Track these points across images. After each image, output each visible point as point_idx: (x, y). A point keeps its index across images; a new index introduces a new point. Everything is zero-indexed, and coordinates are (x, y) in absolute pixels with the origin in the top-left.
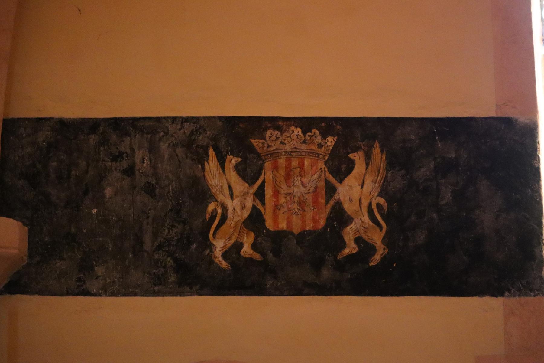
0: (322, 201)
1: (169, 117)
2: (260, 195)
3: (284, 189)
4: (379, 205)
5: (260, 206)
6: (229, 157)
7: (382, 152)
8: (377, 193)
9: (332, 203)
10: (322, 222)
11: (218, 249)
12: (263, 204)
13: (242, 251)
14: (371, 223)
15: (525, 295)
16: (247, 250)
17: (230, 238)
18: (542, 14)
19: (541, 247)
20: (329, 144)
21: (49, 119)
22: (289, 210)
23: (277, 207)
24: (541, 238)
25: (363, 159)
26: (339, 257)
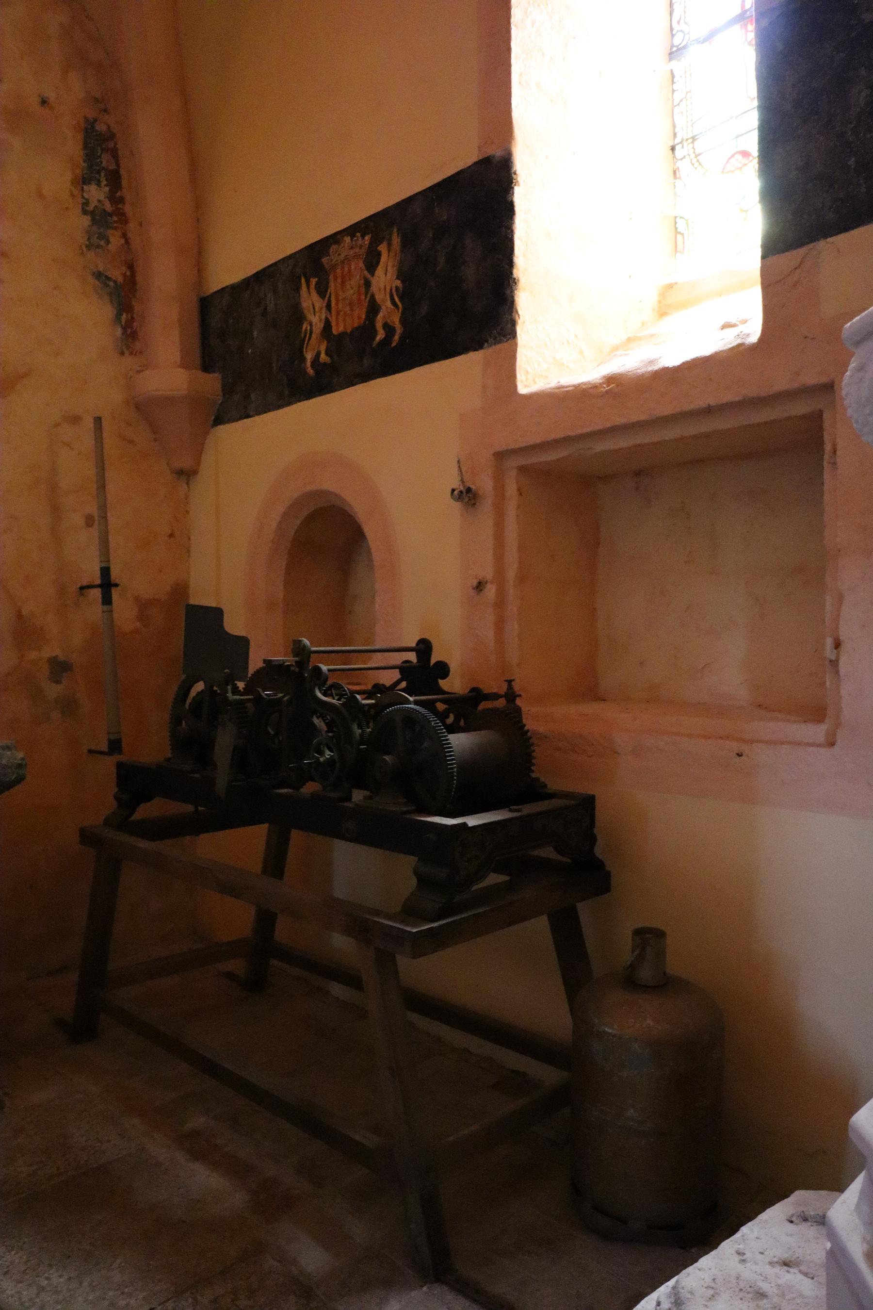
0: (363, 297)
1: (279, 261)
2: (329, 307)
3: (342, 296)
4: (397, 288)
5: (329, 316)
6: (311, 279)
7: (398, 234)
8: (395, 277)
9: (369, 296)
10: (364, 316)
11: (309, 361)
12: (331, 316)
13: (320, 359)
14: (392, 307)
15: (500, 342)
16: (323, 357)
17: (314, 349)
18: (745, 133)
19: (512, 287)
20: (366, 243)
21: (227, 287)
22: (345, 313)
23: (338, 313)
24: (511, 278)
25: (386, 248)
26: (374, 345)
